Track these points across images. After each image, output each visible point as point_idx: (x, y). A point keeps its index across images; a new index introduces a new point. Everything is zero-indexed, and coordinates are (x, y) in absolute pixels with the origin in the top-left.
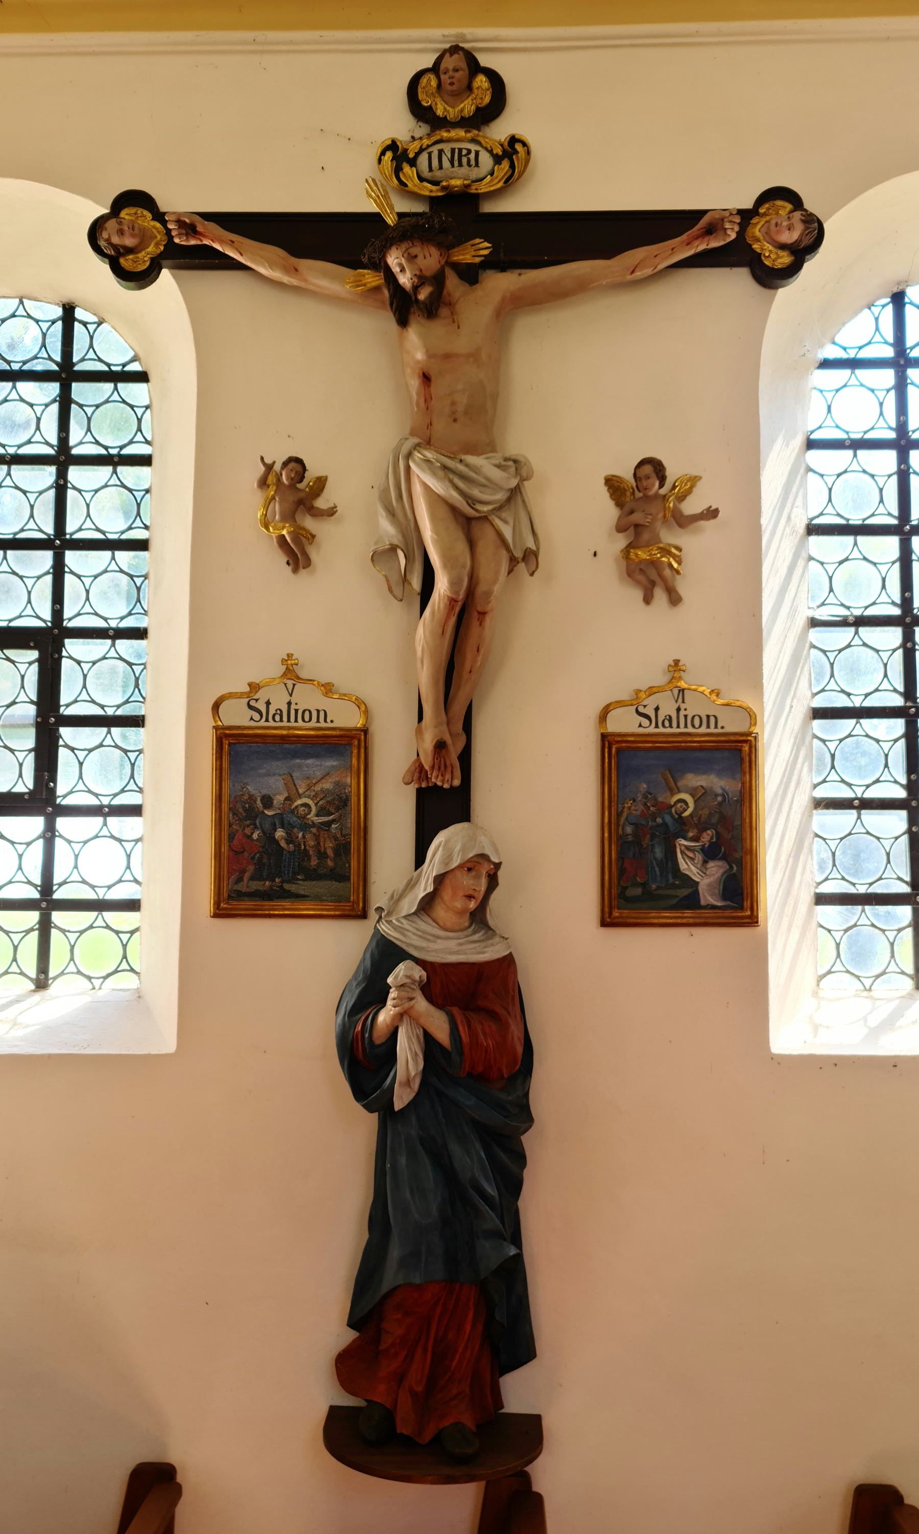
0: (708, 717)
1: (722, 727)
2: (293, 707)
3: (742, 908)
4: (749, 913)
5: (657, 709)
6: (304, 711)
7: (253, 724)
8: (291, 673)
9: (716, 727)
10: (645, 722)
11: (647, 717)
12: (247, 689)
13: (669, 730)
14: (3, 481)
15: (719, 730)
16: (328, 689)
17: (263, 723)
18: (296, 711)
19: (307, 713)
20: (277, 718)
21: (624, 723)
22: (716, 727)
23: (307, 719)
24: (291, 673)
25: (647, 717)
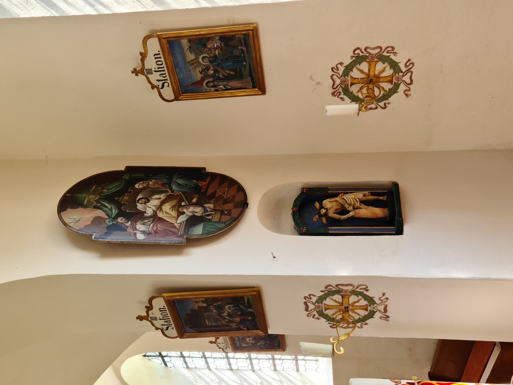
0: (156, 58)
1: (159, 51)
2: (157, 70)
3: (248, 34)
4: (251, 32)
5: (158, 81)
6: (157, 64)
7: (170, 86)
8: (140, 71)
9: (159, 54)
10: (166, 85)
11: (163, 84)
12: (155, 89)
13: (167, 74)
14: (238, 383)
15: (161, 52)
16: (143, 56)
17: (169, 81)
18: (158, 68)
19: (158, 63)
20: (164, 76)
21: (168, 92)
22: (159, 54)
23: (161, 63)
24: (140, 71)
25: (163, 84)
